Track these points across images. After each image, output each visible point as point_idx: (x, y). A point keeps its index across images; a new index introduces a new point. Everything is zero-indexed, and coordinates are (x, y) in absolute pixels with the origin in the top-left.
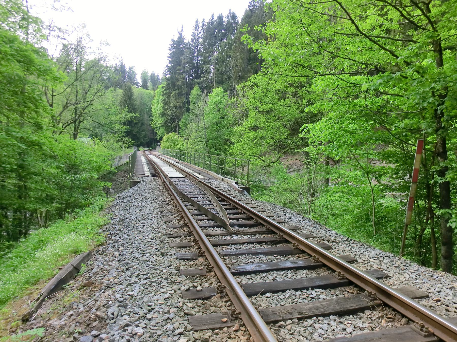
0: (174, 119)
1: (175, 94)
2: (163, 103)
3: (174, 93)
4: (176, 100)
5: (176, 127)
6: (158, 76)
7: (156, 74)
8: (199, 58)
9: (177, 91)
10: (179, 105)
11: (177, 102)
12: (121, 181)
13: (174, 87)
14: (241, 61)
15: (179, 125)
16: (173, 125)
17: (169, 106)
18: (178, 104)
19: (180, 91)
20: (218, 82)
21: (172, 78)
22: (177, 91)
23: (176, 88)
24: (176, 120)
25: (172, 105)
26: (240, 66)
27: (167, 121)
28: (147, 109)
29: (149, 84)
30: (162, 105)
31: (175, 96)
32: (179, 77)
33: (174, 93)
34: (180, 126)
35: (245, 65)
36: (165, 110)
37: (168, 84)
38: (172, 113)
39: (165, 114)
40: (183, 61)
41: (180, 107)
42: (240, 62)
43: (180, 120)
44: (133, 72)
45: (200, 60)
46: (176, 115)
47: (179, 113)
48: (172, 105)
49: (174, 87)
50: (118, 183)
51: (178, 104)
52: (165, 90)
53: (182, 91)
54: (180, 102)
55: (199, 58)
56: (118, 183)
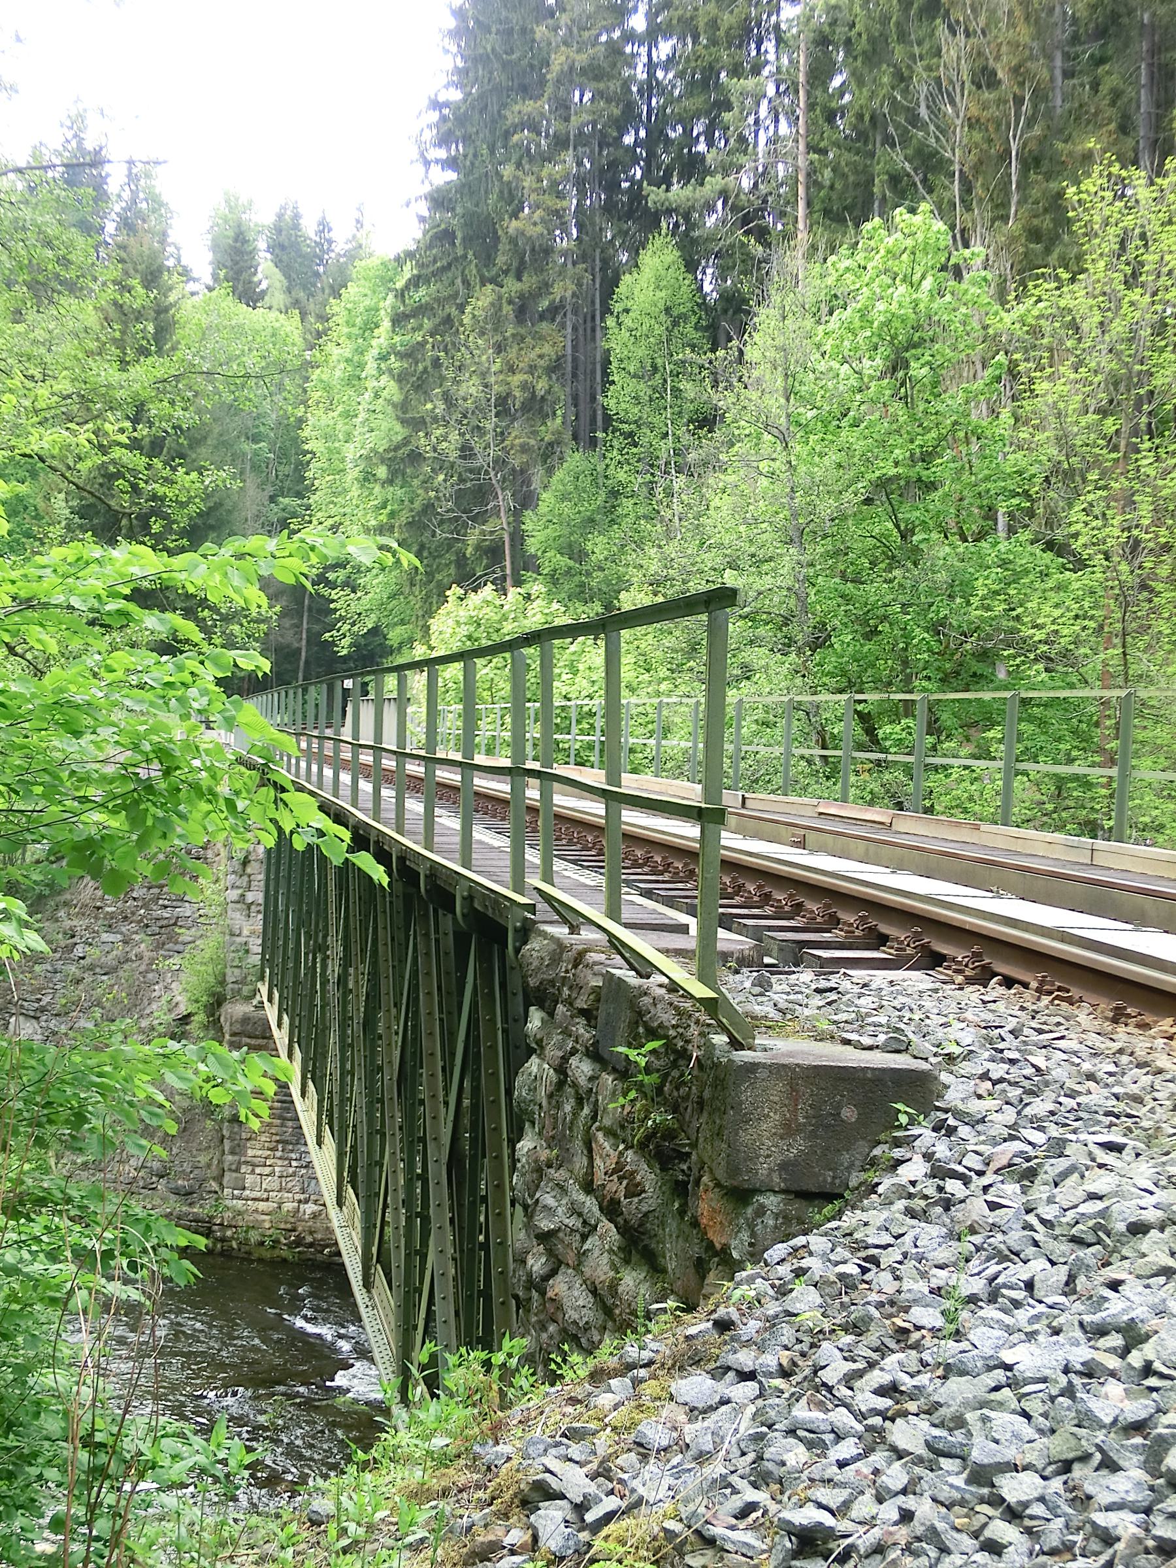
0: (482, 493)
1: (496, 306)
2: (401, 378)
3: (483, 300)
4: (499, 348)
5: (493, 553)
6: (324, 226)
7: (309, 227)
8: (664, 48)
9: (512, 286)
10: (524, 386)
11: (512, 370)
12: (94, 953)
13: (488, 259)
14: (1024, 33)
15: (518, 537)
16: (473, 536)
17: (447, 398)
18: (517, 379)
19: (530, 281)
20: (827, 212)
21: (465, 188)
22: (512, 286)
23: (501, 259)
24: (504, 499)
25: (471, 388)
26: (1015, 70)
27: (428, 508)
28: (256, 439)
29: (267, 273)
30: (392, 389)
31: (497, 321)
32: (528, 182)
33: (483, 300)
34: (532, 546)
35: (1052, 70)
36: (418, 424)
37: (444, 236)
38: (466, 451)
39: (415, 457)
40: (558, 62)
41: (536, 407)
42: (1015, 45)
43: (526, 501)
44: (157, 203)
45: (670, 62)
46: (500, 463)
47: (524, 449)
48: (471, 388)
49: (488, 259)
50: (73, 969)
51: (517, 379)
52: (415, 282)
53: (545, 287)
54: (532, 369)
55: (664, 48)
56: (73, 969)
